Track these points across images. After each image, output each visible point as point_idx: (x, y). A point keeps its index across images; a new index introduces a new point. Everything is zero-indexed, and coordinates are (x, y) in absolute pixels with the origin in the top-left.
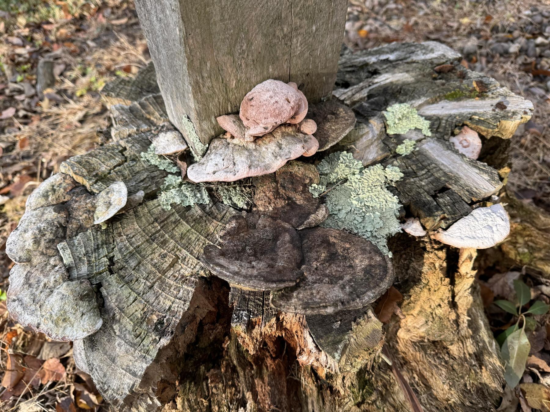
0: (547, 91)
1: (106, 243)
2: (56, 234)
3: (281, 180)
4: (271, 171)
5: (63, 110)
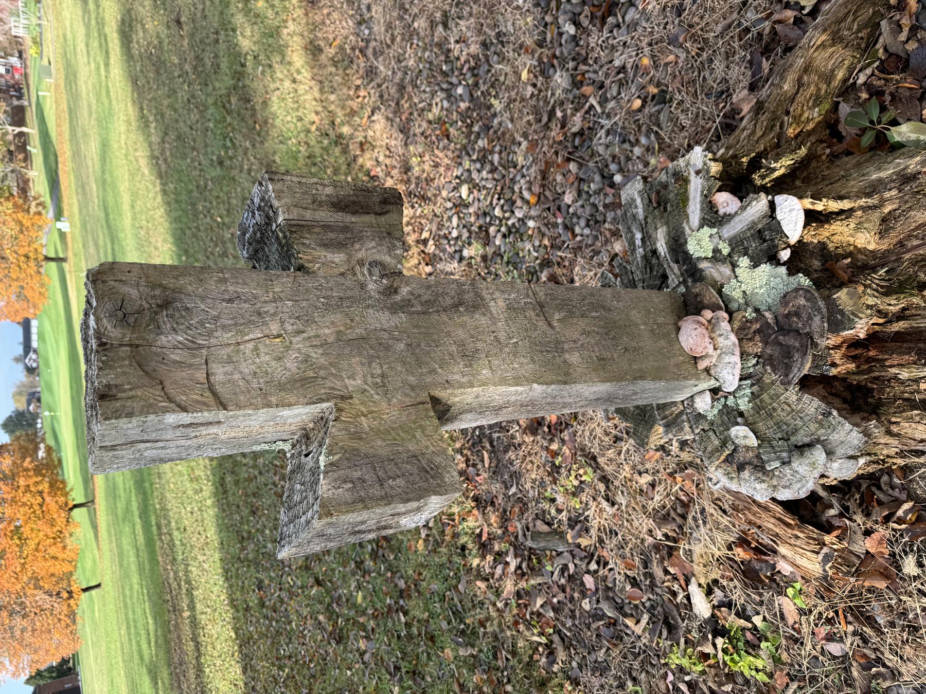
0: (632, 4)
1: (769, 442)
2: (759, 471)
3: (742, 336)
4: (737, 342)
5: (594, 524)
